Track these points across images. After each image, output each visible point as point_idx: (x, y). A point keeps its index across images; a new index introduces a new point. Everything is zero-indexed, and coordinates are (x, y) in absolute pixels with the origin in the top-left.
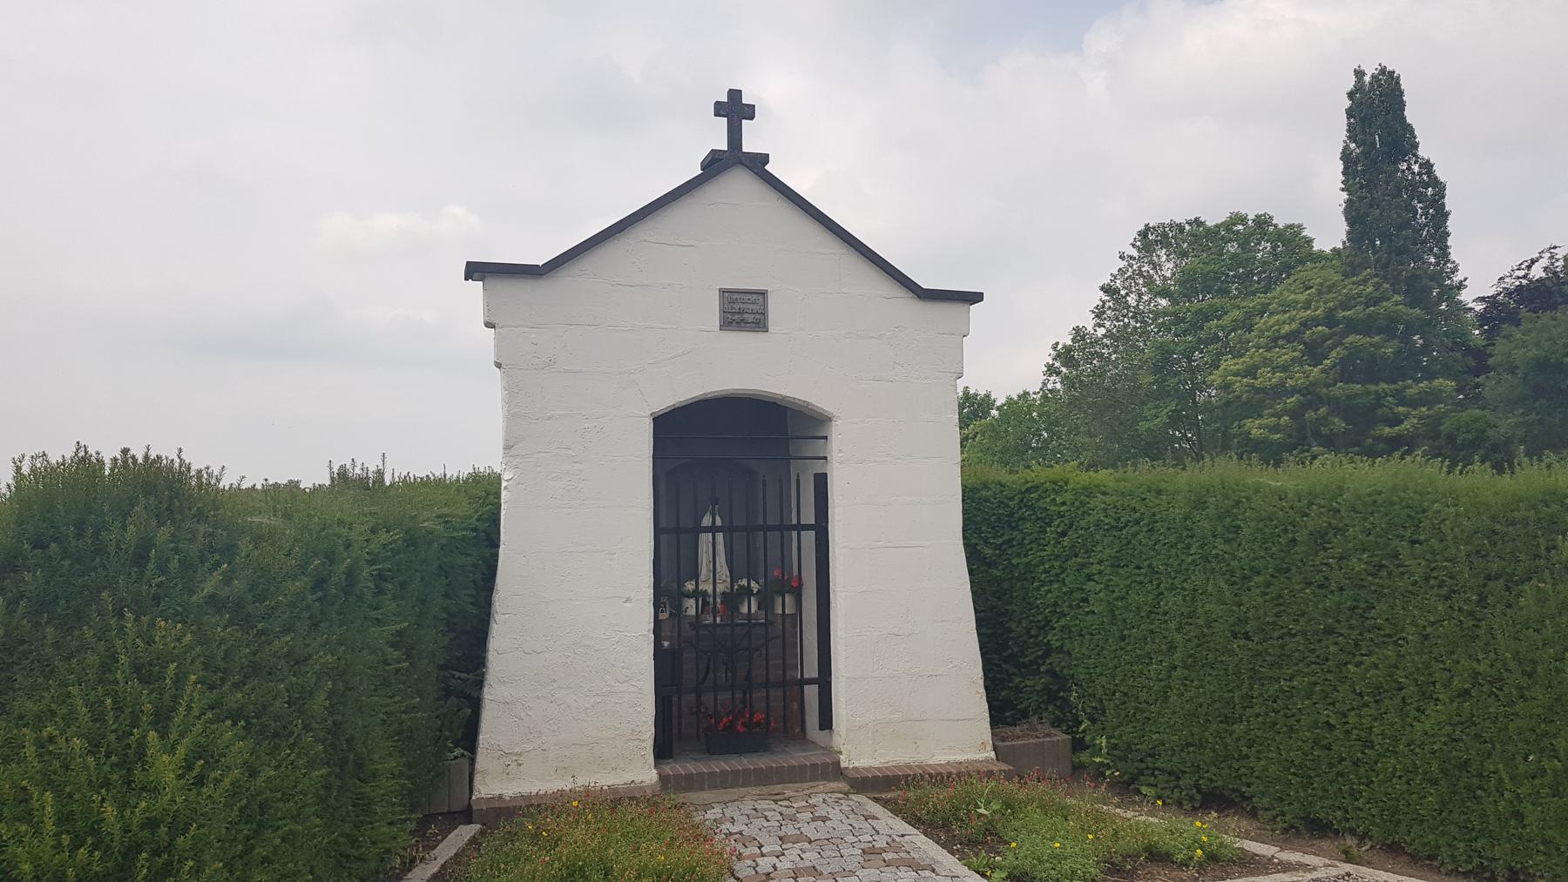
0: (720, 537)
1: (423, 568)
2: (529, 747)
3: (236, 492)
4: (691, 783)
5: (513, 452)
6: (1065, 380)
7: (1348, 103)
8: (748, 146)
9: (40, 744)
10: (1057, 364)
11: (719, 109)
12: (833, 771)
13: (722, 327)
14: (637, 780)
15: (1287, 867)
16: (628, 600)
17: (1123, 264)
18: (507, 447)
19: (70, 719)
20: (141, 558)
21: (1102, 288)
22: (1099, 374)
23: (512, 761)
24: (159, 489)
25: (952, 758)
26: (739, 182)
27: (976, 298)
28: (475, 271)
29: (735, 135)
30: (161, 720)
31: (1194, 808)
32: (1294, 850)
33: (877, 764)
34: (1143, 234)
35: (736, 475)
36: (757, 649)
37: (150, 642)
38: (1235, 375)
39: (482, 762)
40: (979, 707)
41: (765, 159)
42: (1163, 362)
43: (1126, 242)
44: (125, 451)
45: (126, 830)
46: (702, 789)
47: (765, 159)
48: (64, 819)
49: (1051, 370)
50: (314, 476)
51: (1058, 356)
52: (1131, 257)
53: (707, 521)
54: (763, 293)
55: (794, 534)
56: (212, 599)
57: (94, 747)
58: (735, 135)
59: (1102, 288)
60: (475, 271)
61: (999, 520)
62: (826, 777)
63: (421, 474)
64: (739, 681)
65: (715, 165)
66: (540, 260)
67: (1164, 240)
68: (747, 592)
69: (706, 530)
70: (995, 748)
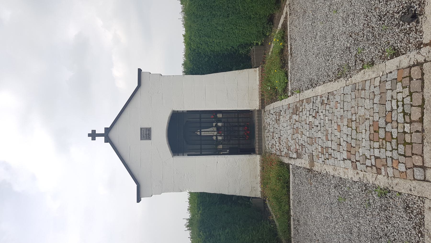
0: (202, 130)
4: (260, 148)
5: (182, 190)
7: (183, 25)
8: (103, 132)
11: (94, 139)
12: (259, 111)
15: (284, 37)
16: (217, 162)
18: (181, 191)
25: (258, 80)
26: (112, 135)
27: (140, 71)
28: (139, 200)
29: (100, 135)
31: (273, 24)
32: (254, 132)
33: (258, 100)
35: (188, 133)
41: (106, 129)
46: (262, 145)
47: (106, 129)
50: (188, 233)
53: (199, 133)
54: (141, 129)
55: (202, 120)
58: (100, 135)
60: (139, 200)
61: (199, 56)
64: (236, 133)
65: (108, 140)
69: (201, 133)
70: (256, 67)
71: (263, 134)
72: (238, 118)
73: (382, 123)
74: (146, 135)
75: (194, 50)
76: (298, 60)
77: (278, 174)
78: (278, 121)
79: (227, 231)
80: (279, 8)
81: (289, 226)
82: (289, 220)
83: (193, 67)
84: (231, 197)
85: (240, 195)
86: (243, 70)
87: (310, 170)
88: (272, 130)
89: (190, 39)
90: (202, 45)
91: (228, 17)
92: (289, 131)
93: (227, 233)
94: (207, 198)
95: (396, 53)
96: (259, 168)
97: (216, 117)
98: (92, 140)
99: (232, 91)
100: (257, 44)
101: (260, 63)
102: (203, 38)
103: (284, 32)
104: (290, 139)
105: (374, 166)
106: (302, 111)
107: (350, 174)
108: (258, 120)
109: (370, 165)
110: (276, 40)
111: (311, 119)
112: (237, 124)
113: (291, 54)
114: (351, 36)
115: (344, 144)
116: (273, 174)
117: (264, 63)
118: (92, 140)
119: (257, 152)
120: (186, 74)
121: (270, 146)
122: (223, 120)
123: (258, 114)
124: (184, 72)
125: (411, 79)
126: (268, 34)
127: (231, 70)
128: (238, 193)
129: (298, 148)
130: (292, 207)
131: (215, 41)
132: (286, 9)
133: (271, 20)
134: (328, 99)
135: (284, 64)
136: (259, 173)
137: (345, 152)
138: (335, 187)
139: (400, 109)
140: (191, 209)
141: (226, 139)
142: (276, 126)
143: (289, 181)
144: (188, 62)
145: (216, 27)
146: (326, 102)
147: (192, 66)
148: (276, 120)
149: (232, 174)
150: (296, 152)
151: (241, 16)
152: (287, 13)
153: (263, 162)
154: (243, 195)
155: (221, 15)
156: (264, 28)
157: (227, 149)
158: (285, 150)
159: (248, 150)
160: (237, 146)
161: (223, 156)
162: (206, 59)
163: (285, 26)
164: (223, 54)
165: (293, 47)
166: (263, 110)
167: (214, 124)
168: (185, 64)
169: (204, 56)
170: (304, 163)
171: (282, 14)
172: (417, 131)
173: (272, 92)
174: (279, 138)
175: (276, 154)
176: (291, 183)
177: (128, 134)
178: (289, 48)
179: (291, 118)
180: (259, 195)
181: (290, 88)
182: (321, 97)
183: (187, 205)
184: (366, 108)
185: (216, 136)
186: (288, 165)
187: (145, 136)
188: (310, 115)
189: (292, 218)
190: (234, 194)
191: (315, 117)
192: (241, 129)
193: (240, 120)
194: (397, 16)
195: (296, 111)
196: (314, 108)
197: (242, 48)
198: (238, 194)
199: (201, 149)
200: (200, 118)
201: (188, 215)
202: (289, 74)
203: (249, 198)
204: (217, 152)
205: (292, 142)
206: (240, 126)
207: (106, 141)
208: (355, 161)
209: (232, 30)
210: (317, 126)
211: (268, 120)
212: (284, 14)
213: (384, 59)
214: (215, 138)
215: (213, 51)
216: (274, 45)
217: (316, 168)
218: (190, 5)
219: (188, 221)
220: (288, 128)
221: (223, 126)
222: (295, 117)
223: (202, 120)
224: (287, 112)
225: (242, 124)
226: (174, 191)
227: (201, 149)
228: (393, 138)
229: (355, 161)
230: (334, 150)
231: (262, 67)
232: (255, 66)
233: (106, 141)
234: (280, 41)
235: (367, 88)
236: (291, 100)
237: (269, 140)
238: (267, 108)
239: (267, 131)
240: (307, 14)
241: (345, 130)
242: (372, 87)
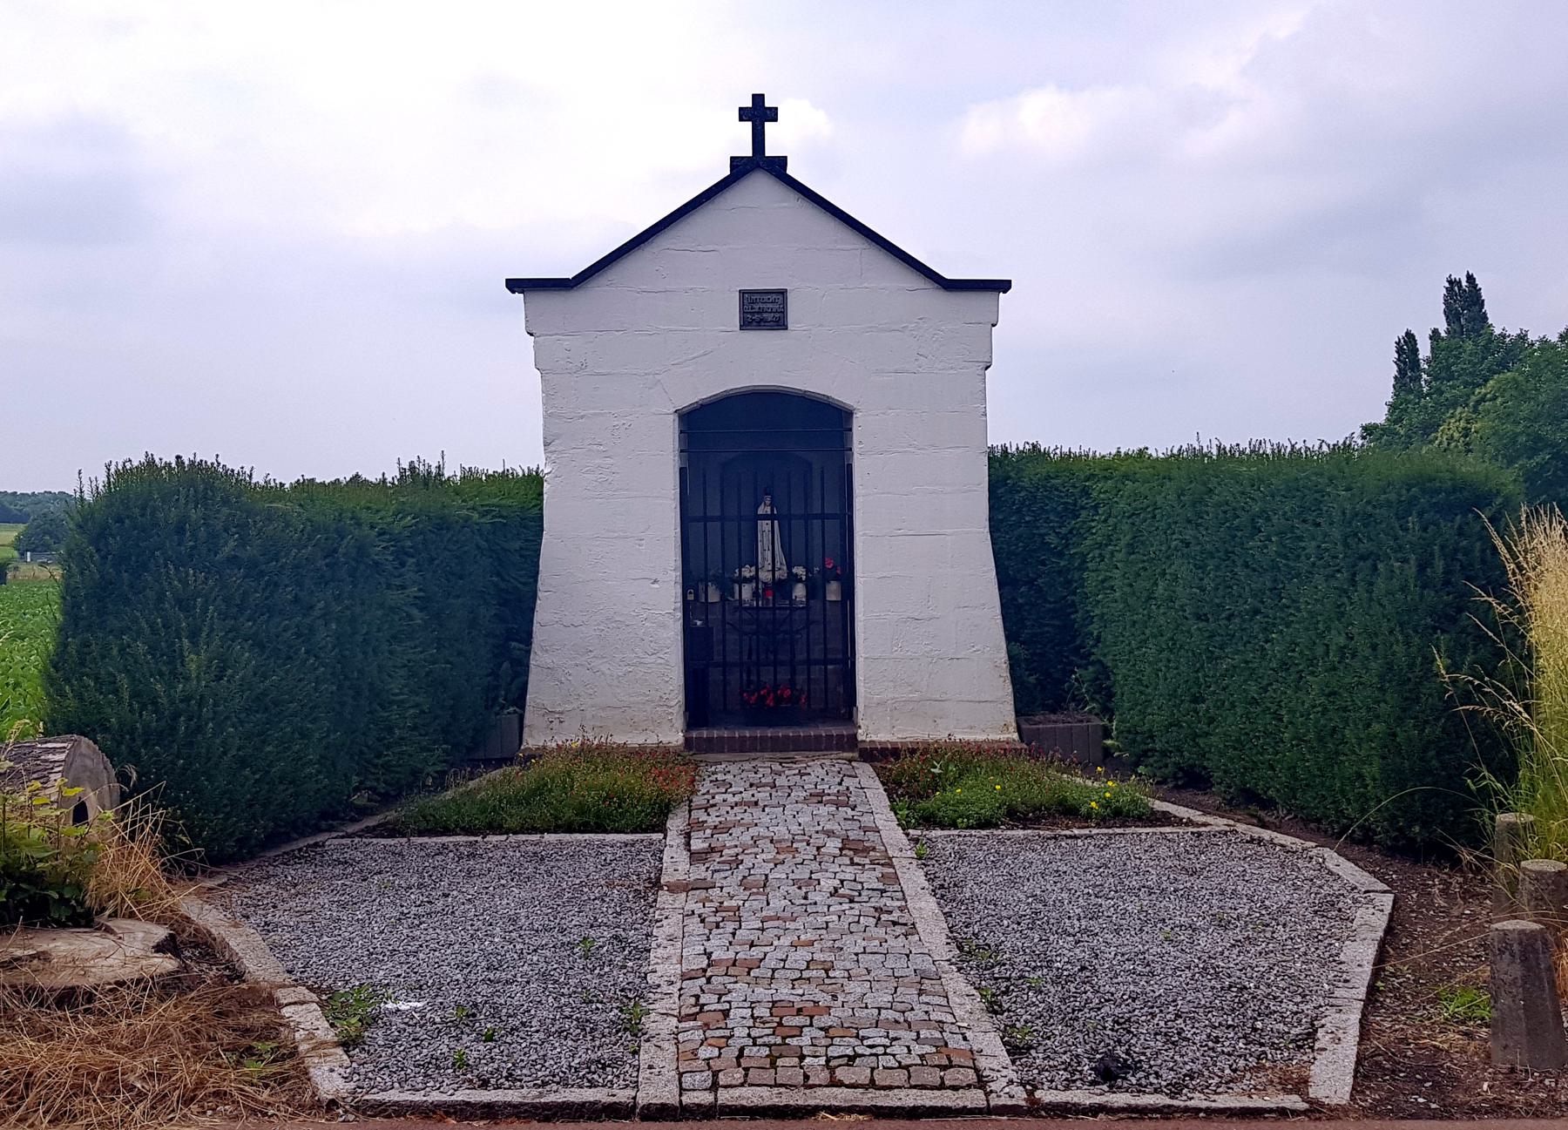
1: (466, 552)
2: (569, 707)
5: (551, 448)
8: (771, 151)
9: (122, 650)
11: (744, 114)
12: (851, 742)
14: (665, 740)
15: (1117, 816)
16: (655, 581)
19: (139, 633)
20: (180, 530)
23: (555, 717)
25: (971, 738)
26: (760, 185)
27: (1005, 286)
28: (514, 285)
30: (194, 636)
33: (894, 739)
35: (767, 473)
36: (798, 632)
39: (529, 718)
40: (1003, 691)
41: (782, 161)
45: (172, 702)
47: (782, 161)
48: (135, 695)
50: (381, 467)
54: (783, 293)
56: (233, 560)
57: (152, 650)
60: (514, 285)
61: (1066, 509)
63: (495, 467)
64: (768, 661)
65: (740, 168)
66: (570, 275)
68: (796, 579)
69: (765, 517)
70: (1019, 730)
71: (766, 755)
75: (1086, 492)
76: (1030, 855)
77: (623, 801)
78: (815, 799)
79: (415, 612)
81: (447, 831)
82: (468, 831)
83: (1023, 488)
84: (522, 633)
85: (533, 669)
86: (1008, 681)
87: (656, 884)
88: (781, 781)
89: (1126, 477)
90: (1105, 521)
91: (1199, 618)
92: (784, 829)
93: (408, 615)
94: (517, 545)
95: (1016, 1051)
96: (635, 740)
98: (741, 109)
99: (928, 632)
100: (1107, 733)
101: (1032, 741)
102: (1125, 527)
103: (1140, 818)
104: (753, 831)
105: (701, 1011)
106: (852, 864)
107: (664, 965)
109: (702, 1001)
110: (1107, 789)
111: (828, 884)
112: (801, 657)
113: (1055, 838)
114: (1083, 968)
115: (756, 953)
116: (623, 778)
117: (1034, 755)
118: (741, 109)
119: (694, 734)
120: (992, 460)
121: (720, 777)
122: (816, 604)
123: (840, 737)
125: (944, 1068)
126: (1141, 769)
127: (1011, 636)
128: (539, 658)
129: (726, 851)
131: (1117, 574)
133: (1190, 781)
134: (895, 923)
135: (1017, 816)
136: (619, 739)
138: (616, 937)
139: (860, 1050)
140: (470, 478)
141: (746, 616)
142: (798, 794)
143: (606, 832)
144: (1043, 470)
145: (1164, 573)
146: (884, 917)
147: (1026, 482)
149: (612, 630)
150: (712, 850)
151: (1202, 666)
152: (1205, 825)
153: (657, 756)
154: (532, 678)
155: (1203, 590)
156: (1164, 754)
157: (706, 621)
158: (712, 820)
159: (698, 709)
160: (717, 658)
162: (1052, 539)
163: (1166, 819)
164: (1073, 604)
165: (1080, 843)
166: (856, 755)
167: (799, 571)
168: (1035, 454)
169: (1063, 531)
170: (676, 864)
171: (1205, 813)
172: (806, 1077)
173: (921, 782)
174: (756, 803)
175: (694, 792)
176: (601, 836)
177: (763, 243)
178: (1076, 832)
179: (830, 834)
181: (936, 833)
182: (901, 909)
183: (490, 464)
184: (862, 996)
185: (756, 578)
187: (756, 307)
188: (842, 882)
189: (479, 839)
190: (535, 646)
191: (835, 892)
192: (784, 675)
193: (816, 671)
194: (1120, 1051)
195: (854, 848)
196: (864, 893)
197: (1097, 679)
199: (705, 519)
200: (823, 517)
202: (984, 832)
203: (520, 700)
204: (691, 580)
205: (746, 838)
206: (793, 673)
207: (735, 161)
208: (708, 974)
209: (1155, 637)
210: (806, 898)
211: (821, 772)
212: (1203, 819)
213: (1006, 1033)
214: (747, 572)
215: (1082, 567)
217: (664, 897)
218: (1236, 477)
219: (434, 470)
221: (793, 608)
222: (833, 846)
223: (817, 523)
225: (801, 679)
226: (548, 416)
227: (705, 519)
228: (784, 1038)
229: (708, 974)
230: (734, 934)
231: (1018, 752)
232: (1025, 726)
233: (735, 161)
234: (1106, 804)
237: (744, 775)
238: (865, 772)
239: (777, 767)
240: (1185, 877)
241: (803, 954)
242: (925, 1008)
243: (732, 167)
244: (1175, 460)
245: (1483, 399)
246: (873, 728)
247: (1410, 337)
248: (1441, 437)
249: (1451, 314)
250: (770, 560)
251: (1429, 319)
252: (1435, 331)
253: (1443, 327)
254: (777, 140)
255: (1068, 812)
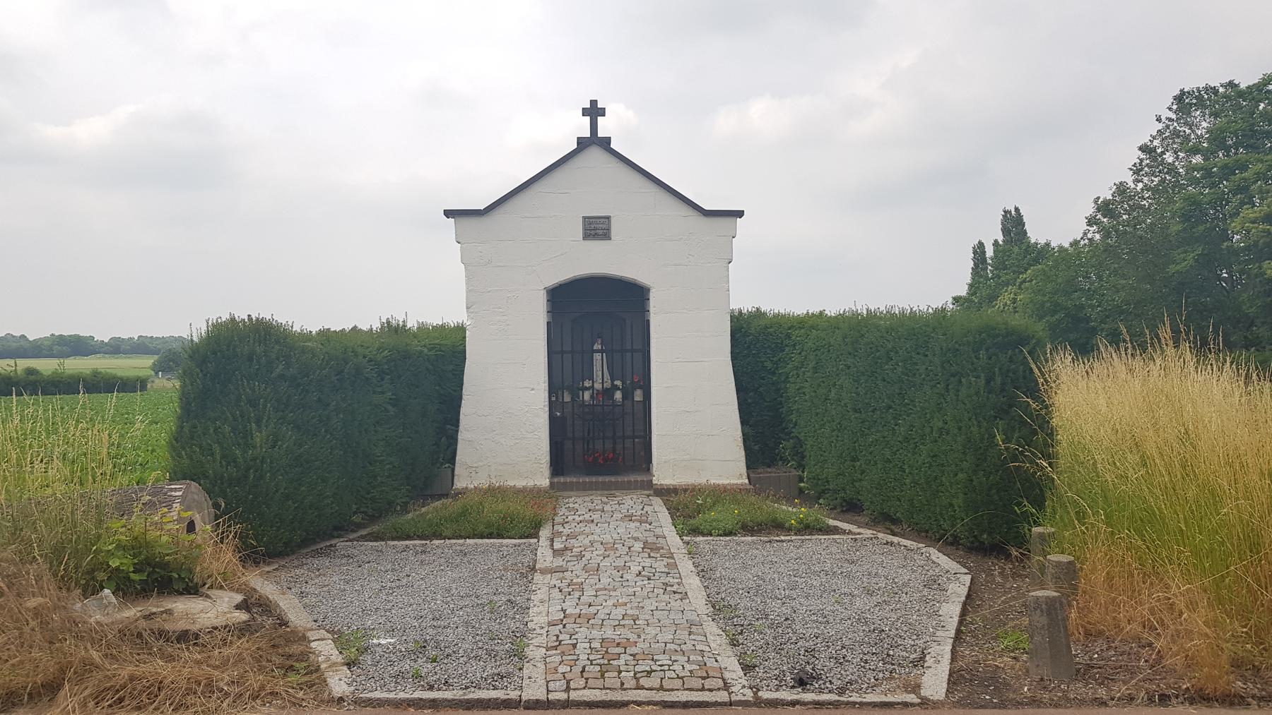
1: (419, 375)
3: (301, 334)
6: (1106, 233)
10: (1099, 216)
11: (585, 112)
12: (649, 485)
13: (584, 238)
15: (807, 528)
17: (1160, 126)
21: (1140, 149)
22: (1135, 223)
24: (263, 335)
26: (595, 153)
27: (740, 214)
28: (448, 213)
30: (258, 422)
32: (601, 475)
34: (1180, 98)
35: (598, 323)
37: (254, 391)
38: (1253, 222)
39: (458, 470)
42: (1193, 212)
43: (1163, 105)
44: (1013, 224)
48: (223, 457)
49: (1091, 221)
50: (370, 321)
51: (1098, 210)
52: (1170, 120)
54: (608, 218)
55: (629, 354)
56: (282, 376)
59: (1140, 149)
60: (448, 213)
62: (642, 488)
64: (600, 436)
65: (583, 144)
67: (1201, 103)
69: (598, 351)
72: (634, 437)
73: (631, 650)
74: (595, 229)
75: (788, 336)
76: (755, 552)
79: (390, 407)
80: (873, 521)
81: (409, 538)
82: (420, 538)
87: (533, 569)
89: (812, 327)
91: (856, 411)
94: (451, 367)
95: (747, 668)
96: (520, 483)
97: (635, 386)
99: (695, 420)
107: (538, 617)
108: (629, 482)
110: (801, 513)
111: (635, 569)
122: (629, 403)
124: (740, 312)
125: (704, 678)
126: (821, 501)
127: (744, 422)
130: (448, 542)
131: (807, 385)
132: (868, 533)
133: (850, 508)
135: (748, 529)
137: (577, 611)
142: (618, 515)
144: (763, 323)
147: (753, 331)
148: (632, 515)
149: (506, 421)
150: (566, 549)
154: (459, 446)
155: (858, 394)
156: (835, 491)
158: (566, 531)
159: (558, 464)
160: (570, 435)
161: (130, 331)
162: (768, 365)
163: (835, 531)
167: (618, 383)
168: (758, 314)
170: (545, 556)
173: (691, 509)
175: (555, 514)
177: (595, 189)
179: (636, 539)
180: (460, 484)
183: (434, 319)
186: (536, 536)
192: (609, 445)
193: (628, 443)
194: (809, 668)
195: (651, 548)
198: (461, 436)
199: (562, 352)
200: (632, 351)
201: (412, 324)
203: (452, 460)
204: (554, 388)
205: (587, 542)
206: (615, 444)
211: (631, 502)
214: (587, 384)
216: (793, 512)
217: (538, 577)
220: (615, 536)
221: (614, 405)
222: (638, 546)
224: (647, 534)
225: (619, 447)
226: (468, 291)
227: (562, 352)
231: (748, 491)
234: (801, 521)
235: (692, 637)
236: (673, 539)
238: (658, 503)
239: (605, 499)
240: (846, 565)
241: (619, 612)
243: (578, 144)
244: (841, 318)
245: (1024, 281)
246: (663, 474)
247: (981, 244)
248: (999, 304)
249: (1005, 231)
250: (600, 375)
251: (992, 234)
252: (996, 241)
253: (1000, 239)
254: (605, 127)
255: (778, 526)
